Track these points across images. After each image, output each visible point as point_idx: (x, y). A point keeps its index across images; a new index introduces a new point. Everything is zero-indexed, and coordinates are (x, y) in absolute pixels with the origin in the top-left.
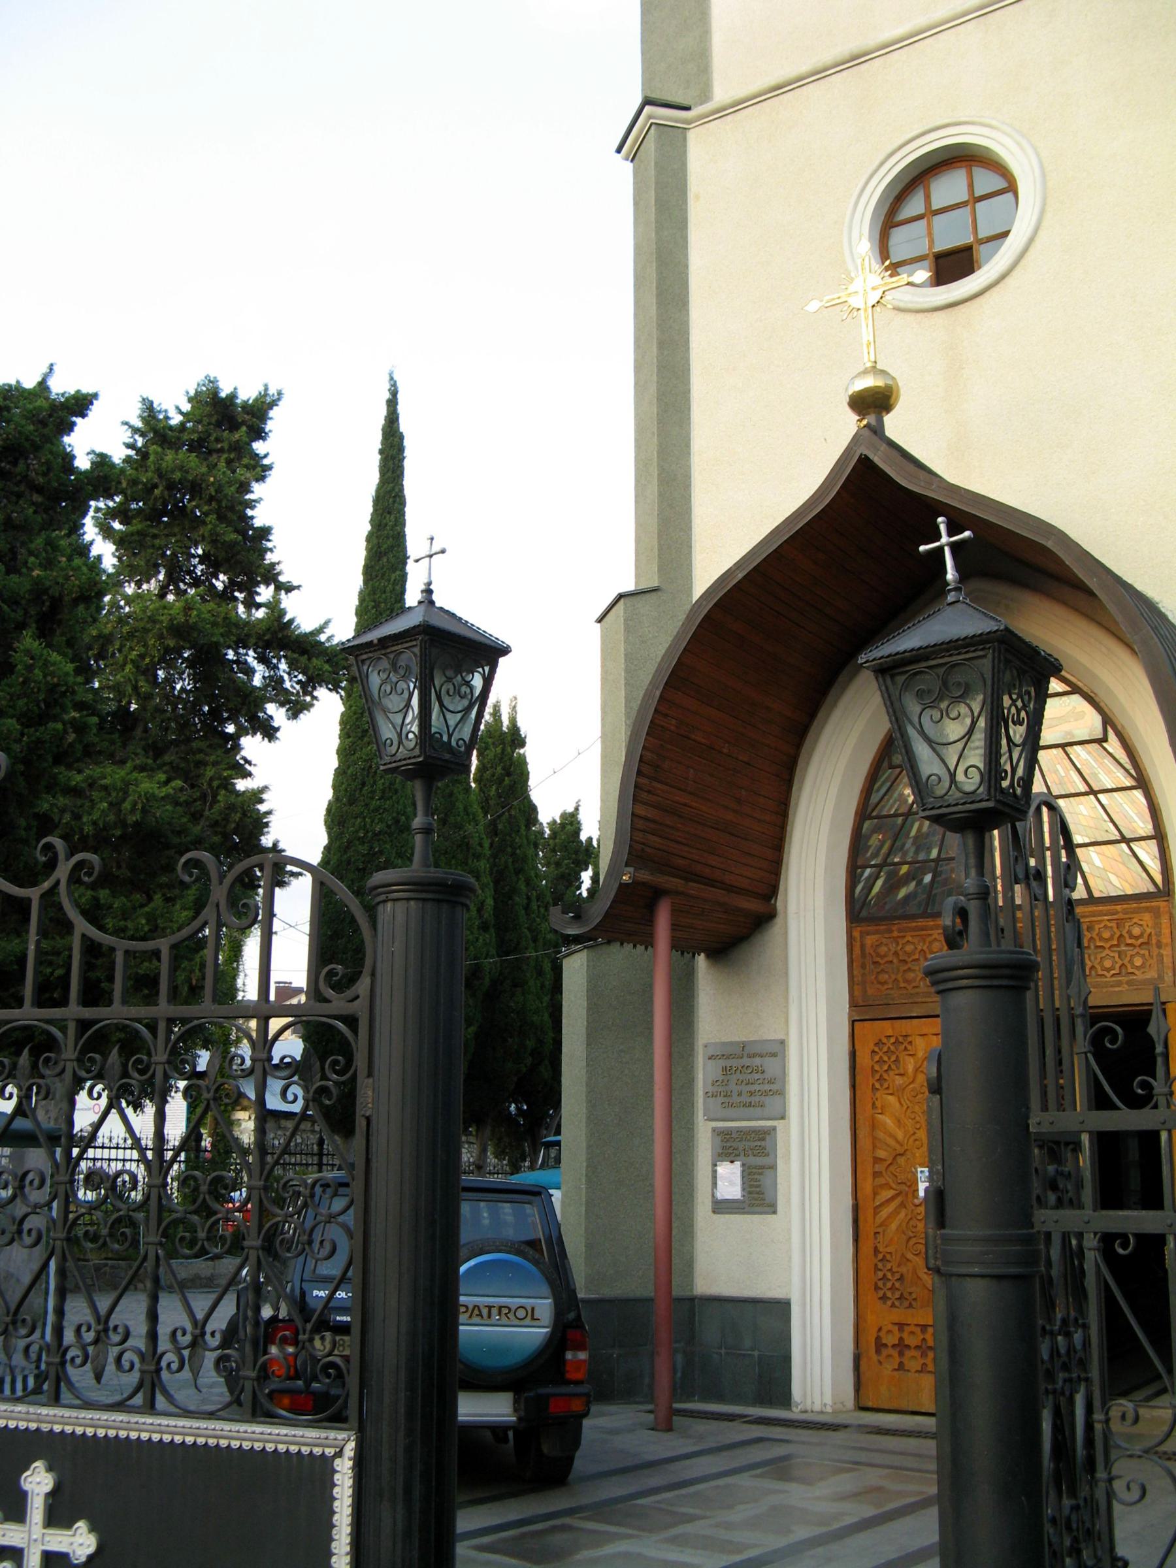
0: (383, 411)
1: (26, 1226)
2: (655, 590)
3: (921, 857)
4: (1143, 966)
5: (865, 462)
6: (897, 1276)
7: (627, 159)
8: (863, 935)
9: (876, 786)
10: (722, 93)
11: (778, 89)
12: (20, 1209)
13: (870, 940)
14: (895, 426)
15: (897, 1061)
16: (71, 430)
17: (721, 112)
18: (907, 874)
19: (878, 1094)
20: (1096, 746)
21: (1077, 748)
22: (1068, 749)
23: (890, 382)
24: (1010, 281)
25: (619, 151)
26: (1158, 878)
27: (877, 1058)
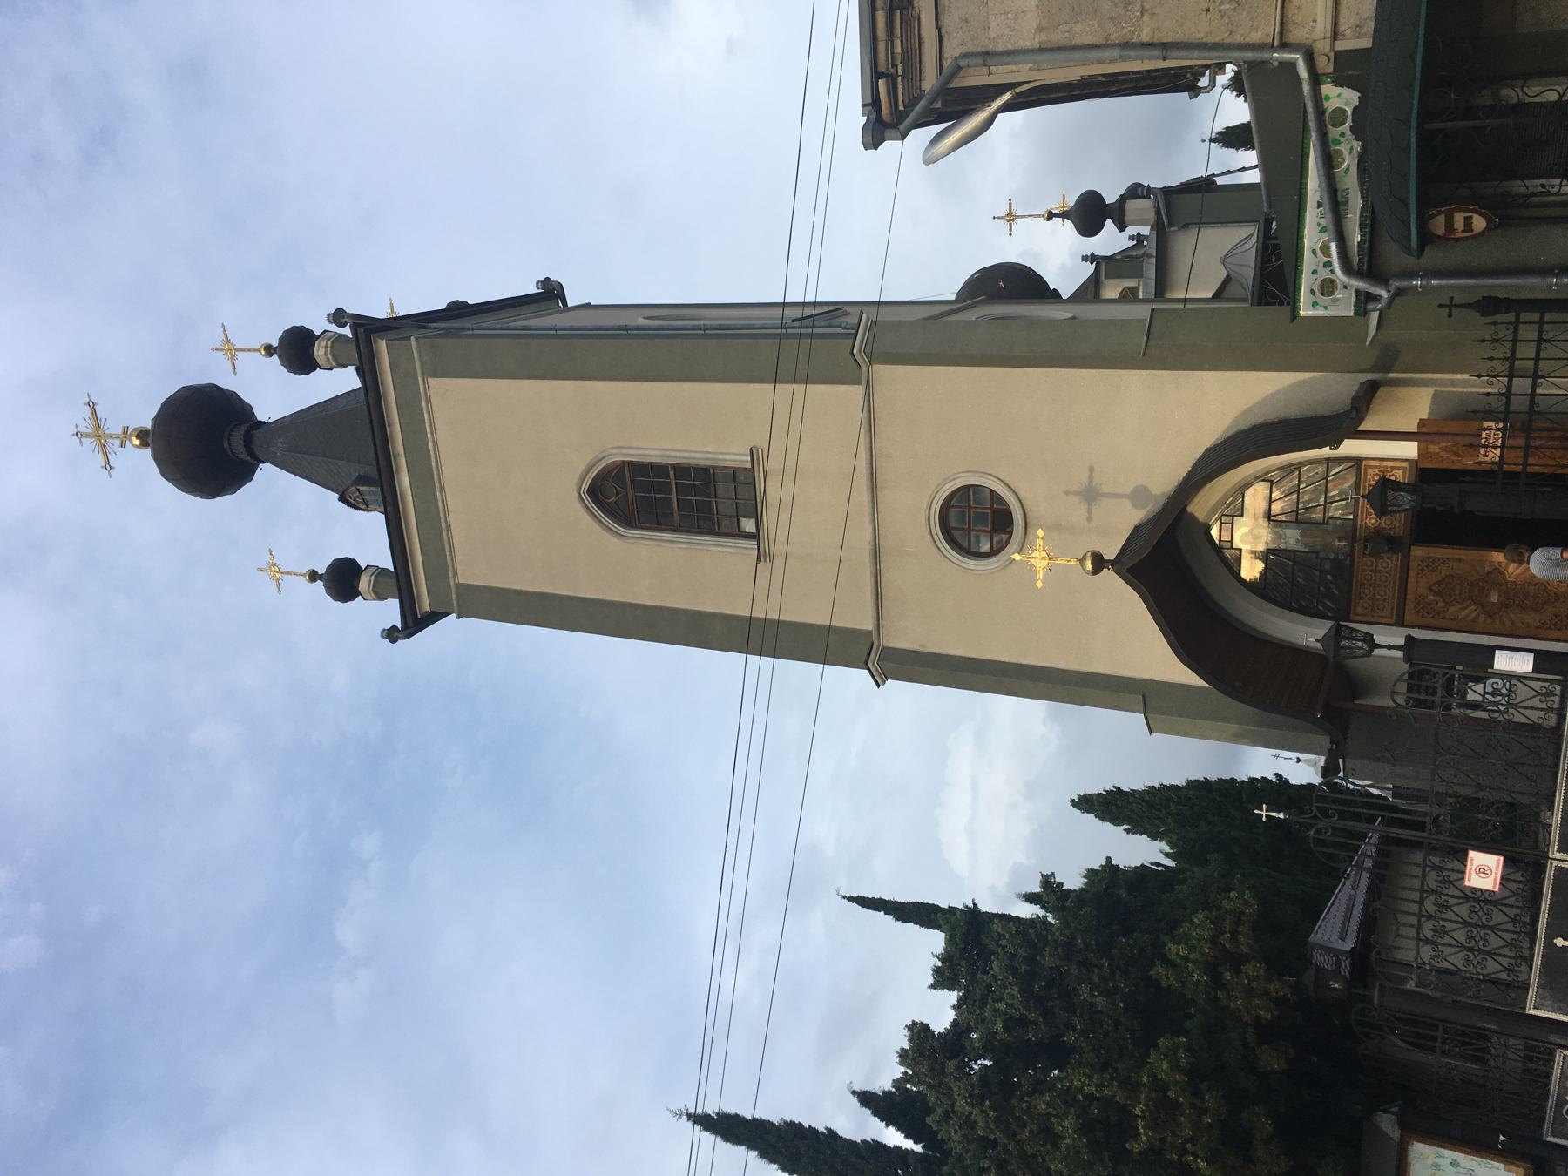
0: (880, 917)
1: (1483, 936)
2: (1143, 696)
3: (1317, 579)
4: (1374, 475)
5: (1130, 571)
6: (1554, 618)
7: (884, 683)
8: (1356, 614)
9: (1273, 597)
10: (868, 625)
11: (877, 595)
12: (1475, 962)
13: (1359, 610)
14: (1110, 554)
15: (1429, 605)
16: (865, 1140)
17: (879, 626)
18: (1325, 587)
19: (1447, 616)
20: (1274, 486)
21: (1273, 495)
22: (1273, 499)
23: (1089, 554)
24: (1022, 494)
25: (879, 686)
26: (1350, 464)
27: (1426, 615)
